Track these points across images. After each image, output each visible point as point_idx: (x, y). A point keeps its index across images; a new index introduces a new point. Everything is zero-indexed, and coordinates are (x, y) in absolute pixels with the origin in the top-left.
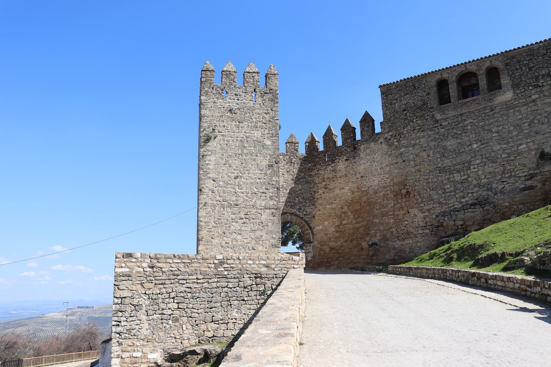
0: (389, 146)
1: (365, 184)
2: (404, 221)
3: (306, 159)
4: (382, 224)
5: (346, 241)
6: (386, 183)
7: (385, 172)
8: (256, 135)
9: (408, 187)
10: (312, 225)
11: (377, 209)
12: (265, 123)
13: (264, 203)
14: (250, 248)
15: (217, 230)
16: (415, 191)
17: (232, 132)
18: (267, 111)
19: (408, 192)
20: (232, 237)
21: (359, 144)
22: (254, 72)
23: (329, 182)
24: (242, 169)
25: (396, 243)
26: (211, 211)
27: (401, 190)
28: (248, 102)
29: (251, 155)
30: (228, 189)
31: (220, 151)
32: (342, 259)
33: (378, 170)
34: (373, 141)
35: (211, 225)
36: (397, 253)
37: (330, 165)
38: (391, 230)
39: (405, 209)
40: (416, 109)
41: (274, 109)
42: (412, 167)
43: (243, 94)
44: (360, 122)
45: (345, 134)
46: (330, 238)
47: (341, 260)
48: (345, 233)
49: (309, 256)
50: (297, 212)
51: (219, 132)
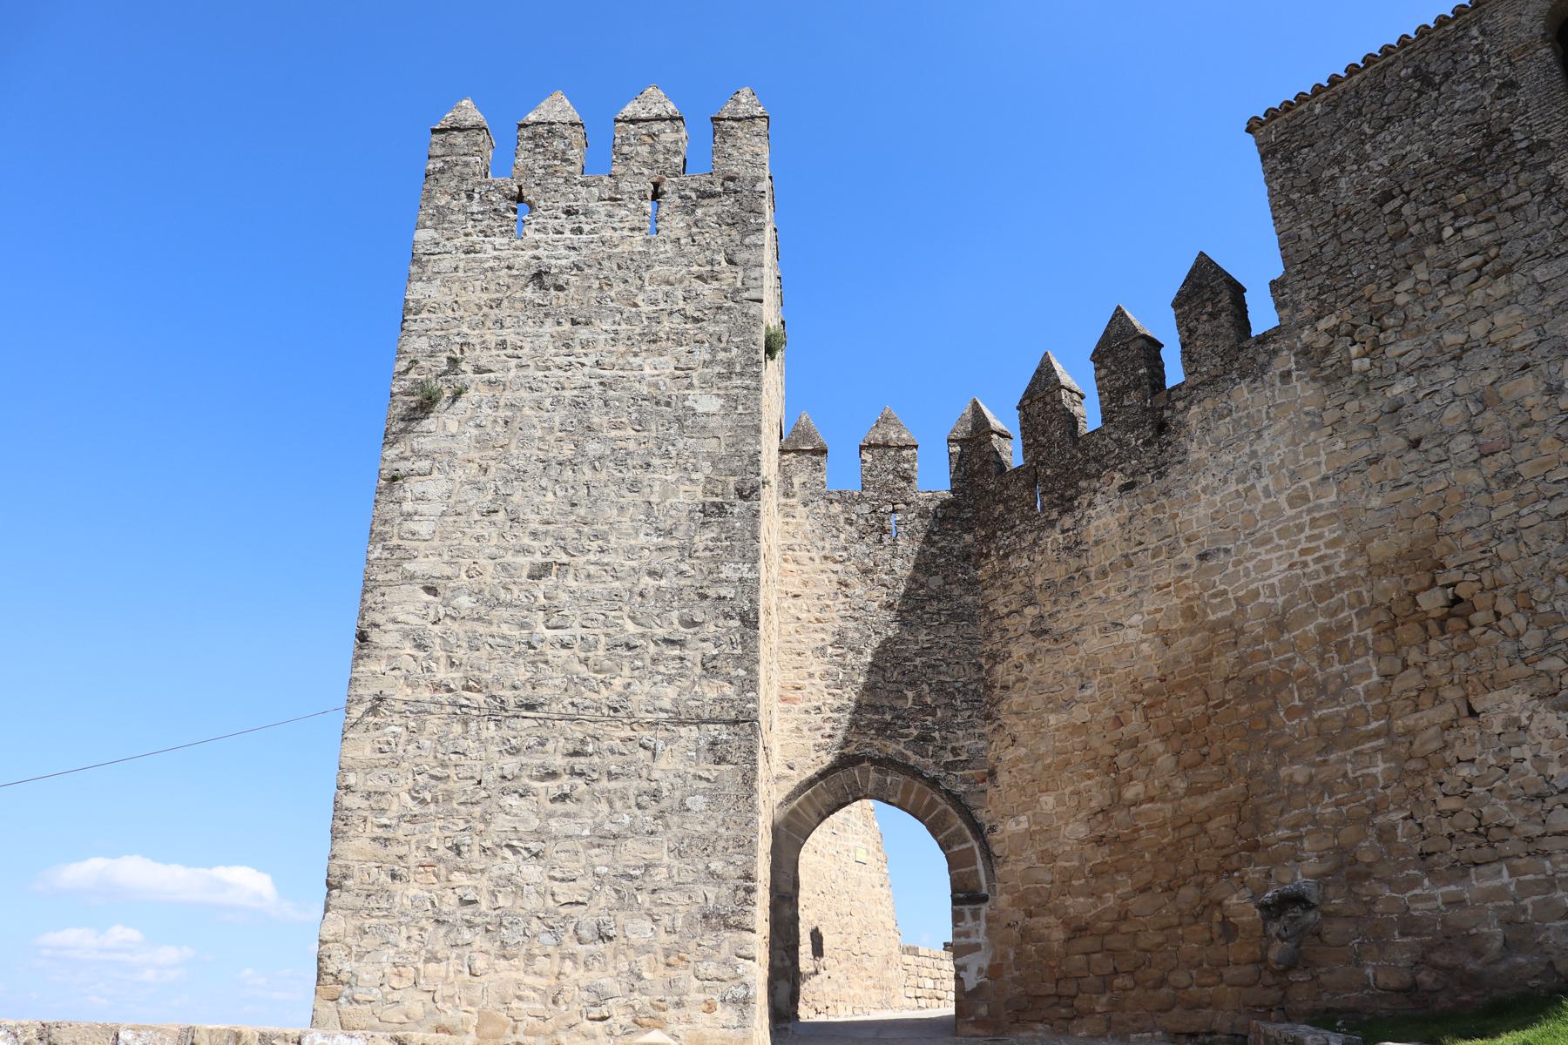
0: (1327, 380)
1: (1222, 587)
2: (1448, 766)
3: (952, 512)
4: (1328, 788)
5: (1143, 890)
6: (1327, 570)
7: (1317, 515)
8: (648, 371)
9: (1454, 575)
10: (982, 816)
11: (1291, 713)
12: (696, 320)
13: (671, 692)
14: (584, 933)
15: (419, 836)
16: (1499, 592)
17: (538, 368)
18: (709, 268)
19: (1457, 600)
20: (495, 872)
21: (1180, 405)
22: (659, 118)
23: (1055, 602)
24: (570, 533)
25: (1418, 891)
26: (402, 741)
27: (1413, 595)
28: (622, 238)
29: (621, 463)
30: (494, 629)
31: (474, 455)
32: (1129, 982)
33: (1280, 511)
34: (1243, 377)
35: (395, 807)
36: (1431, 948)
37: (1052, 524)
38: (1379, 820)
39: (1452, 693)
40: (1447, 177)
41: (741, 256)
42: (1465, 467)
43: (602, 209)
44: (1176, 305)
45: (1114, 373)
46: (1067, 877)
47: (1124, 990)
48: (1136, 846)
49: (973, 969)
50: (909, 753)
51: (479, 370)
